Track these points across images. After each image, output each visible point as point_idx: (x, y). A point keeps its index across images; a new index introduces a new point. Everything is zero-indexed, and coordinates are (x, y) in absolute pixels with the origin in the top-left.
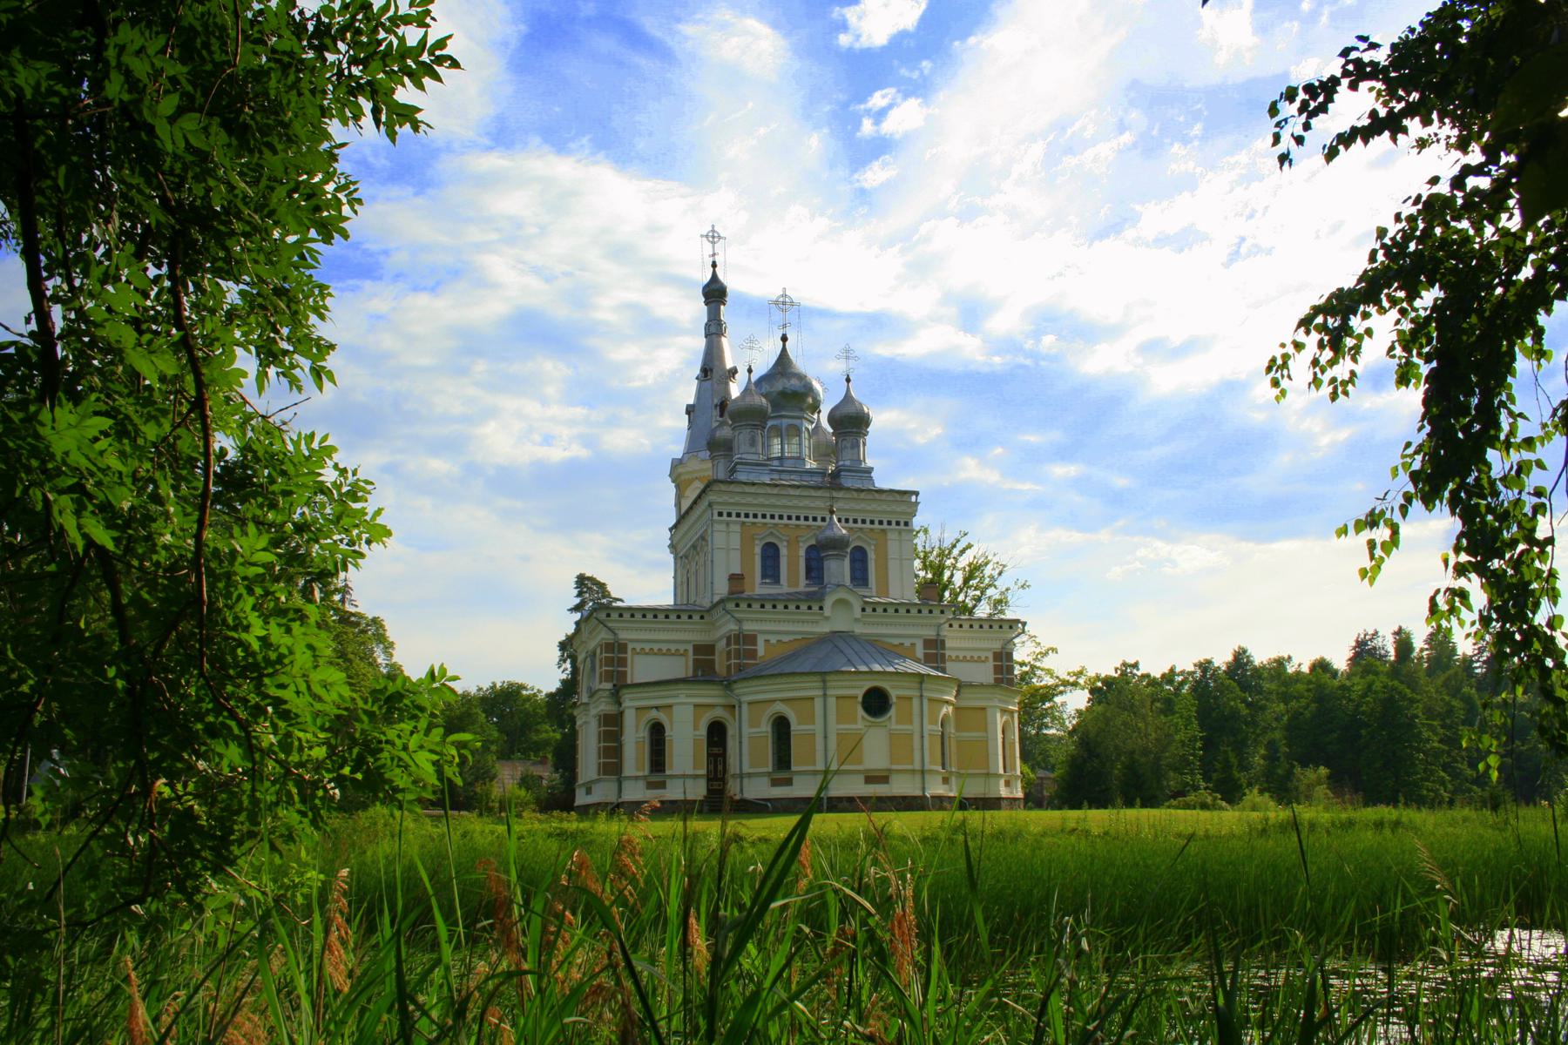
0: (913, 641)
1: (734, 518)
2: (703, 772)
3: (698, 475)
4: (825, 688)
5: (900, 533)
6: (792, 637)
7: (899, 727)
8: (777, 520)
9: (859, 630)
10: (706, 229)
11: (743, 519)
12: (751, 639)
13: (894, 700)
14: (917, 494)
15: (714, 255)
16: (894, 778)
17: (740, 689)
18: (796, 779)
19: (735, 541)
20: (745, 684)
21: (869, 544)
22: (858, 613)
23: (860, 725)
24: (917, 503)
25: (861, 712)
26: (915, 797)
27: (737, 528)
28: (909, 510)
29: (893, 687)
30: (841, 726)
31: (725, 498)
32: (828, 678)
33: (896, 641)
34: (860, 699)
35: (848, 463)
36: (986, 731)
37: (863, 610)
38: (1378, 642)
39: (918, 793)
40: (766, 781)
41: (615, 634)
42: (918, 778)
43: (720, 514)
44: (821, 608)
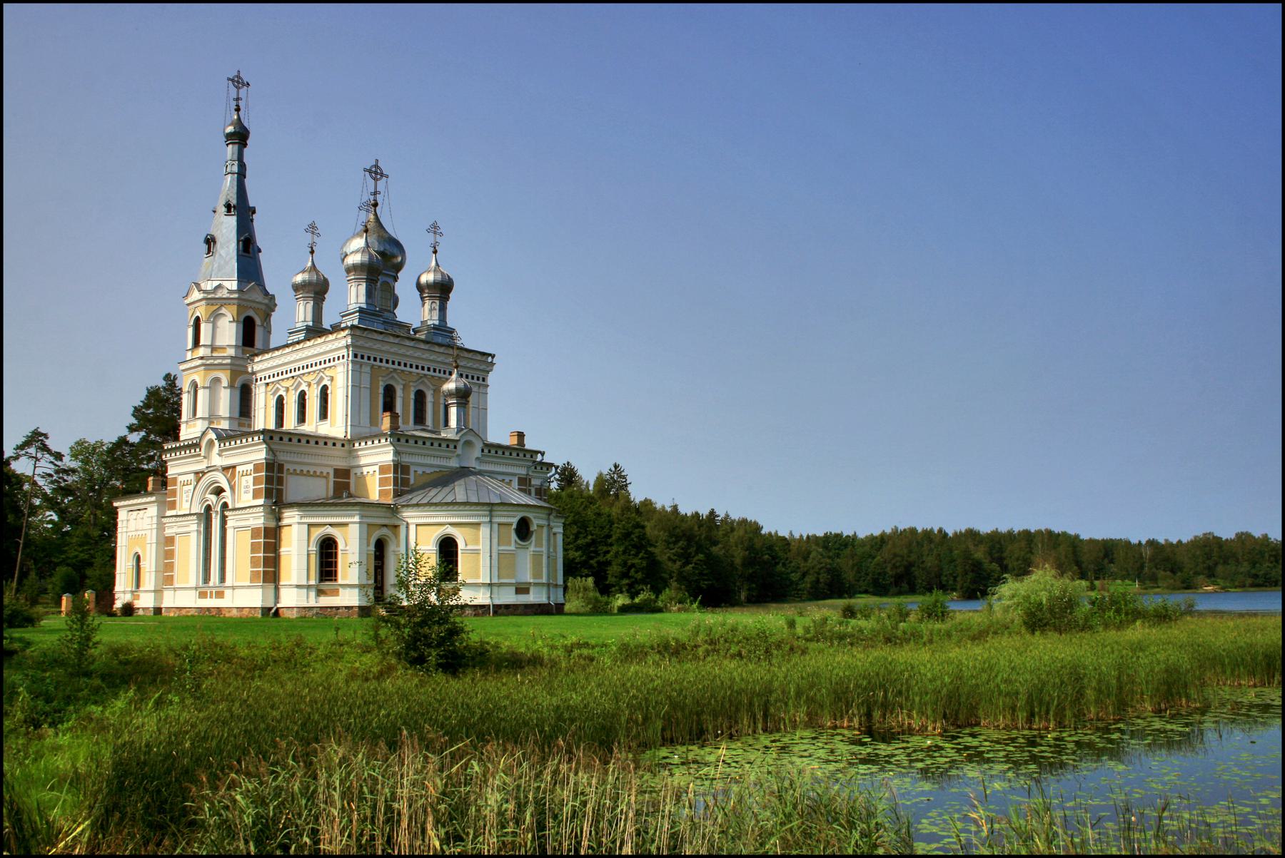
0: (511, 478)
1: (365, 360)
2: (372, 582)
3: (254, 305)
4: (491, 516)
5: (361, 366)
6: (432, 470)
10: (232, 74)
11: (372, 361)
14: (493, 356)
20: (410, 509)
21: (428, 388)
24: (492, 364)
25: (514, 536)
26: (544, 605)
27: (368, 369)
28: (488, 369)
30: (501, 548)
32: (495, 508)
34: (514, 526)
37: (483, 451)
39: (546, 602)
41: (275, 456)
44: (455, 447)
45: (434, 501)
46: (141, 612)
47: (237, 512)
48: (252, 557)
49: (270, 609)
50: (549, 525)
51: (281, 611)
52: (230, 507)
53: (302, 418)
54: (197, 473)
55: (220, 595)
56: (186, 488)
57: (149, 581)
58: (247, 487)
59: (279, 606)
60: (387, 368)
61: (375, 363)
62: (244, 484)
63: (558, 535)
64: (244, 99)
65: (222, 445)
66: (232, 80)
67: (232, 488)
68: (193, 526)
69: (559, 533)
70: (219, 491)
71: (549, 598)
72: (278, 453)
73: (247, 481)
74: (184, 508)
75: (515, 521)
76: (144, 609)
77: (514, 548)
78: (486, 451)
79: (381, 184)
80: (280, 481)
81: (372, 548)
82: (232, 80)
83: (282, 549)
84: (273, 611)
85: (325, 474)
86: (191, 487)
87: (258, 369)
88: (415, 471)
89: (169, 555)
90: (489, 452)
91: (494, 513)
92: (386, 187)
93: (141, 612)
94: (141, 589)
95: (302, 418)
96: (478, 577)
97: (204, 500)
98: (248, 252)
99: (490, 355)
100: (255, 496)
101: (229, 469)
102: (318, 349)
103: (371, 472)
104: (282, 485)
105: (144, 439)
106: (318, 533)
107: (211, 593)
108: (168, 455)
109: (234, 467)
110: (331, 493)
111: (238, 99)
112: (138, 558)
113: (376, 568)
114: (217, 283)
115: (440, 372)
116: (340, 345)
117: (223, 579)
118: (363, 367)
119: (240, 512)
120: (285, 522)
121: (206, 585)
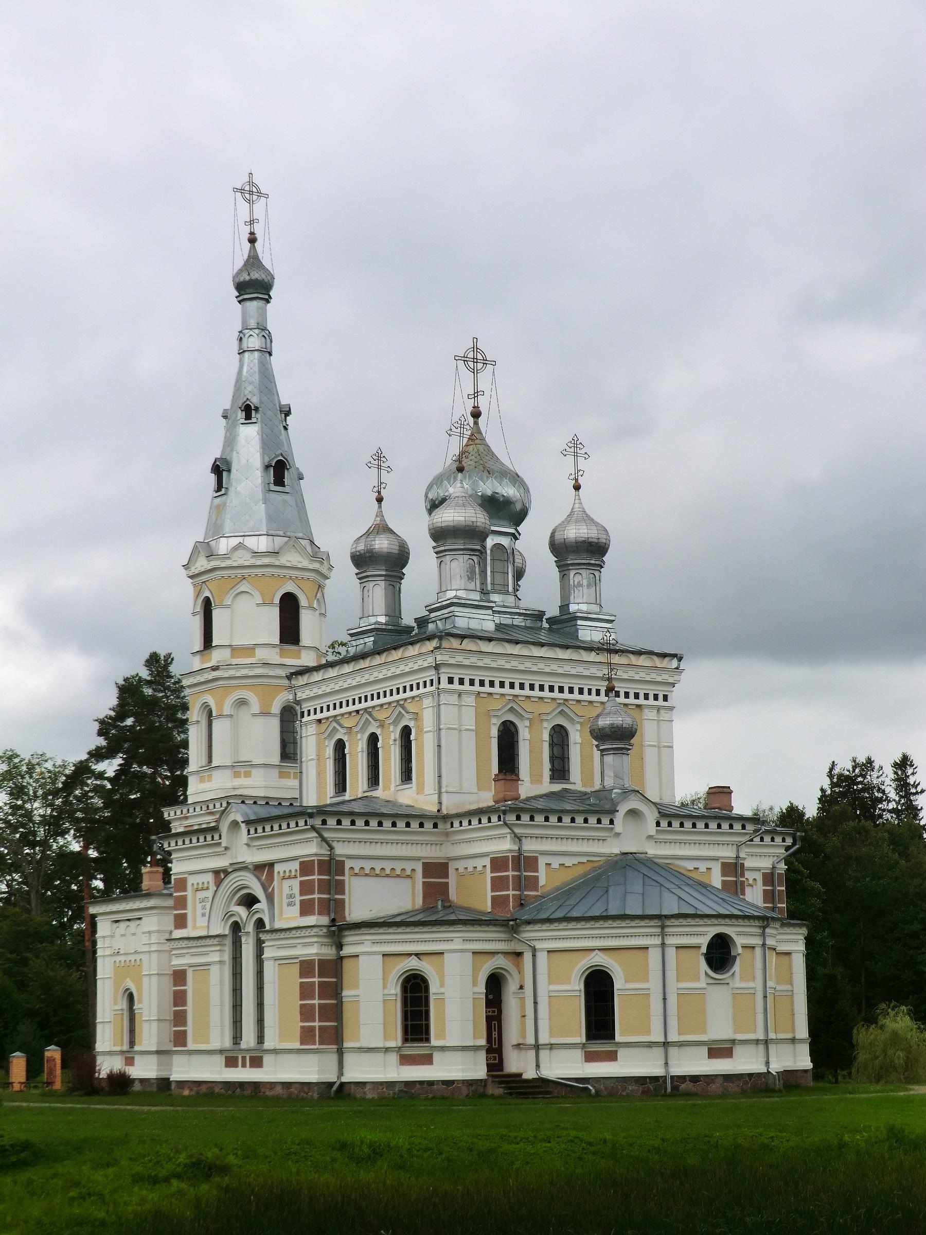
0: (709, 864)
2: (483, 1042)
3: (294, 573)
4: (663, 935)
5: (460, 695)
6: (575, 860)
7: (743, 985)
8: (517, 691)
9: (653, 850)
10: (240, 181)
12: (531, 862)
13: (740, 950)
15: (252, 222)
16: (738, 1050)
17: (529, 933)
18: (621, 1053)
19: (469, 718)
22: (652, 829)
23: (702, 984)
25: (704, 966)
26: (759, 1074)
27: (470, 700)
28: (671, 680)
29: (739, 934)
30: (553, 987)
31: (459, 659)
32: (668, 923)
33: (690, 865)
35: (584, 607)
36: (792, 984)
37: (658, 824)
38: (873, 778)
40: (578, 1054)
41: (331, 848)
42: (761, 1048)
43: (451, 681)
44: (612, 822)
45: (575, 914)
46: (137, 1087)
47: (278, 936)
48: (302, 1006)
49: (331, 1084)
50: (764, 945)
51: (346, 1088)
52: (268, 928)
53: (374, 780)
54: (216, 872)
55: (257, 1062)
56: (201, 895)
57: (149, 1038)
58: (291, 896)
59: (344, 1079)
60: (503, 695)
61: (482, 689)
62: (286, 891)
63: (794, 956)
64: (262, 221)
65: (252, 831)
66: (242, 191)
67: (270, 898)
68: (219, 956)
69: (797, 952)
70: (249, 901)
71: (767, 1063)
72: (334, 844)
73: (291, 887)
74: (197, 926)
75: (704, 941)
76: (142, 1081)
77: (703, 985)
78: (664, 824)
79: (485, 377)
80: (340, 887)
81: (482, 988)
82: (242, 191)
83: (345, 993)
84: (335, 1088)
85: (408, 873)
86: (209, 894)
87: (304, 697)
88: (548, 865)
89: (180, 998)
90: (670, 824)
91: (667, 930)
92: (494, 381)
93: (137, 1087)
94: (136, 1048)
95: (374, 780)
96: (648, 1032)
97: (228, 915)
98: (282, 484)
99: (674, 656)
100: (306, 908)
101: (264, 869)
102: (393, 669)
103: (479, 868)
104: (343, 893)
105: (123, 770)
106: (395, 970)
107: (244, 1058)
108: (173, 843)
109: (271, 865)
110: (419, 902)
111: (252, 222)
112: (131, 997)
113: (489, 1019)
114: (234, 542)
115: (590, 693)
116: (426, 664)
117: (261, 1038)
118: (464, 696)
119: (282, 935)
120: (347, 951)
121: (236, 1047)
